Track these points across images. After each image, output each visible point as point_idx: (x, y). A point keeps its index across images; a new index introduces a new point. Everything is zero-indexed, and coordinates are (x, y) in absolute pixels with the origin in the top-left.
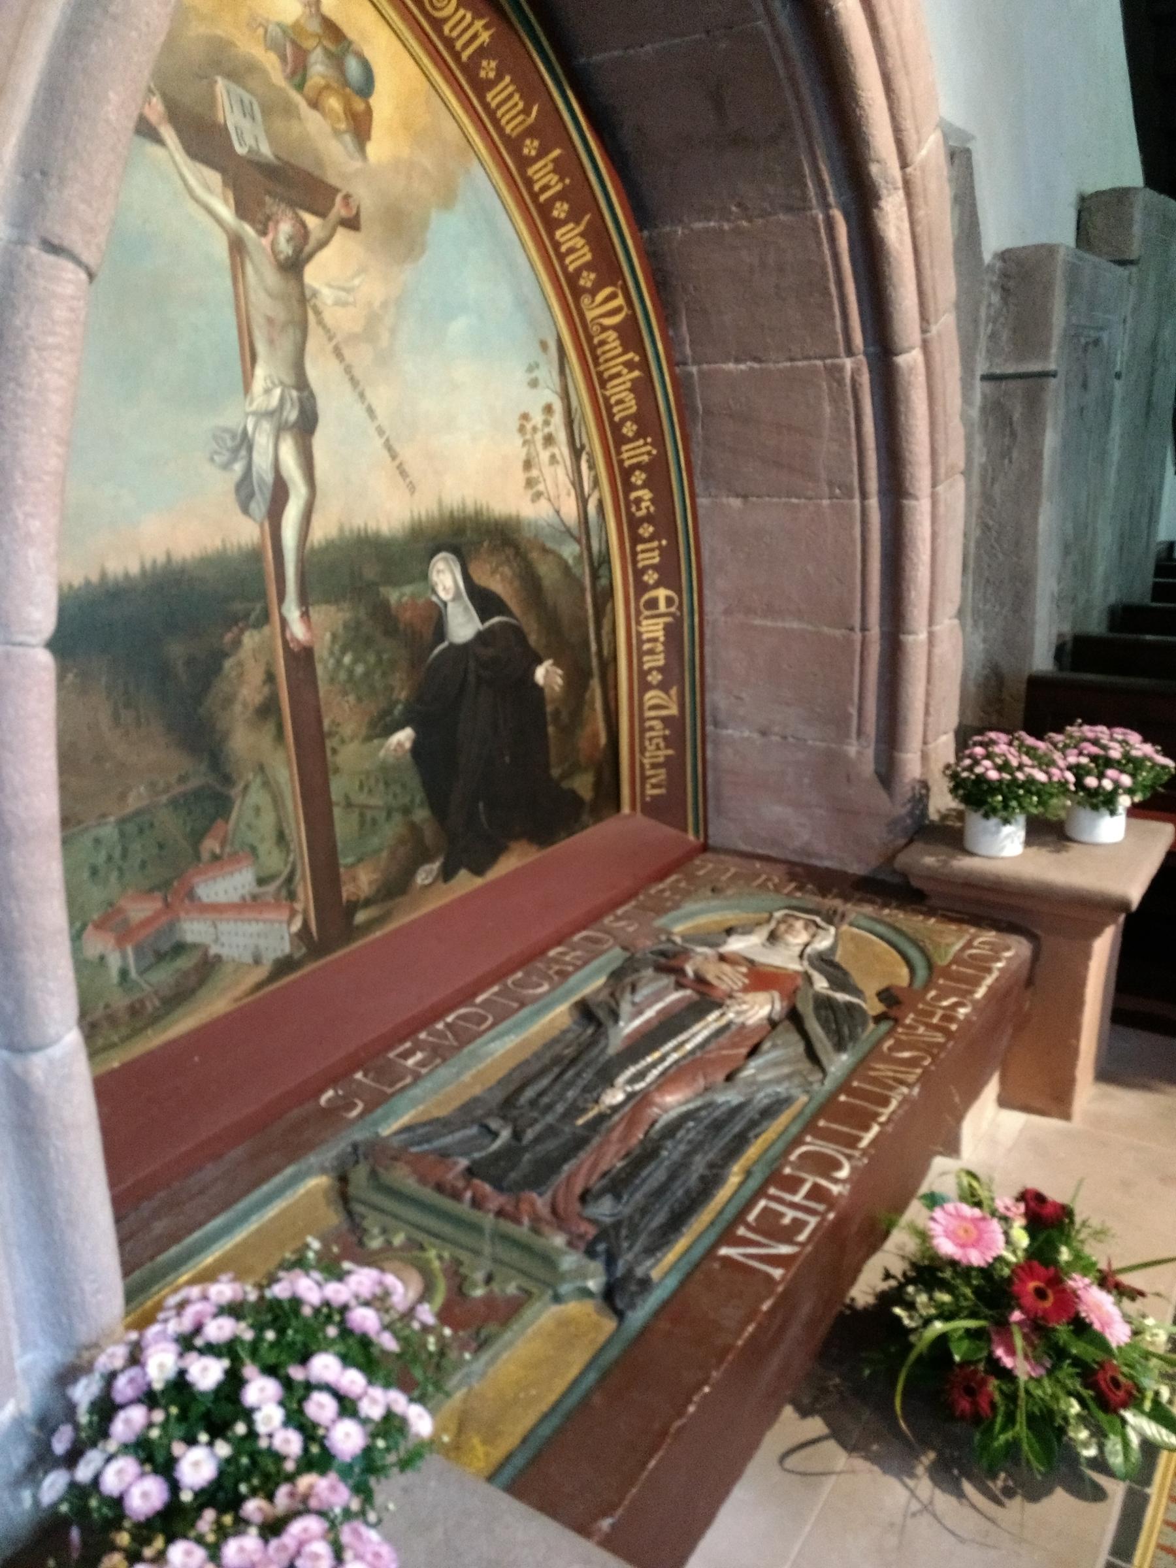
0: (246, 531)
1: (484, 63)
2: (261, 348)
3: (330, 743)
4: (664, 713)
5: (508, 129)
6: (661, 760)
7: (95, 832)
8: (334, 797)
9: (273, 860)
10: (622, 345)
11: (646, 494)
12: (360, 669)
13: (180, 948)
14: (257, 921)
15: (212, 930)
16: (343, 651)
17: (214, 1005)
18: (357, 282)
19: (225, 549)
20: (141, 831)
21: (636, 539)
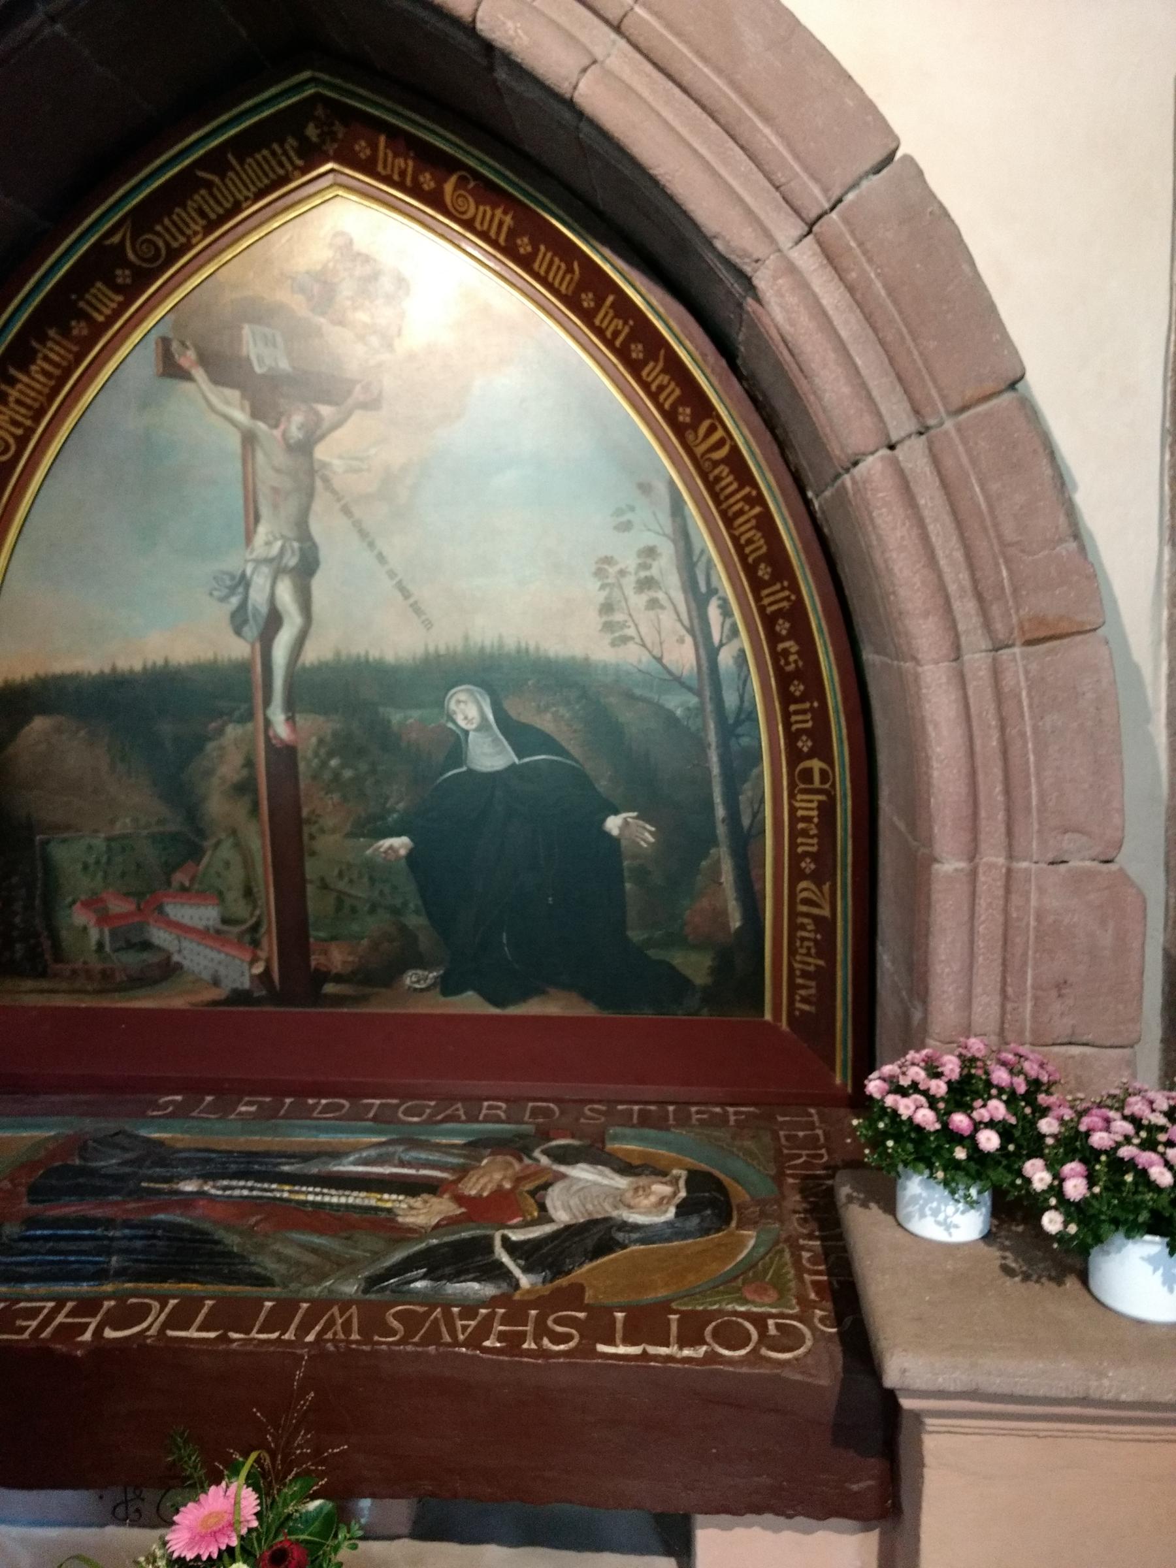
0: (238, 649)
1: (519, 242)
2: (265, 510)
3: (306, 830)
4: (815, 911)
5: (563, 289)
6: (812, 968)
8: (308, 877)
9: (240, 909)
10: (736, 479)
12: (348, 774)
13: (147, 946)
15: (176, 942)
16: (331, 754)
20: (124, 849)
21: (787, 698)
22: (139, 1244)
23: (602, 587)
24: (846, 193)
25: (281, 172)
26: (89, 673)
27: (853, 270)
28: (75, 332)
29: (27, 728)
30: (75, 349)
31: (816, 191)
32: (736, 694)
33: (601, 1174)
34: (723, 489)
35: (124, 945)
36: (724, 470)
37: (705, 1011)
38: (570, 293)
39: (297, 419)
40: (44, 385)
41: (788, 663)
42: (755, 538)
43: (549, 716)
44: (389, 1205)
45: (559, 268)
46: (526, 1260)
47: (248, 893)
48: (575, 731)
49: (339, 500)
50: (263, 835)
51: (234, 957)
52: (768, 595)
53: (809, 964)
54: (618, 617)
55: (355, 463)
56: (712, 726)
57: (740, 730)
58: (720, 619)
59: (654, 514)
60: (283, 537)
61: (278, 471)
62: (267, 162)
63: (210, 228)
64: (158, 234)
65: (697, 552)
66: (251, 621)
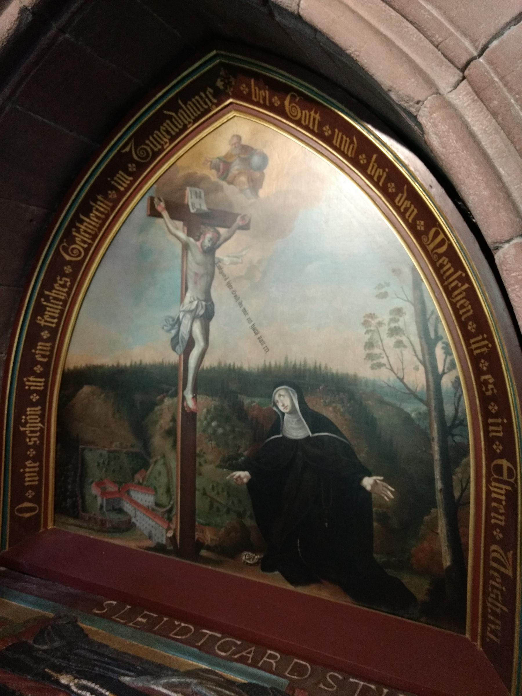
0: (173, 357)
1: (324, 129)
2: (190, 285)
3: (198, 460)
4: (503, 570)
6: (498, 611)
8: (197, 486)
9: (164, 499)
10: (452, 266)
12: (220, 431)
13: (121, 511)
15: (134, 511)
16: (213, 419)
18: (244, 253)
20: (115, 459)
21: (487, 414)
23: (367, 332)
24: (490, 41)
25: (206, 107)
26: (108, 366)
27: (494, 99)
28: (110, 196)
30: (111, 204)
31: (467, 44)
34: (445, 272)
35: (111, 509)
36: (445, 260)
38: (353, 156)
39: (209, 236)
40: (97, 223)
41: (487, 390)
42: (466, 305)
43: (331, 409)
45: (346, 141)
47: (168, 491)
48: (346, 420)
49: (226, 279)
52: (474, 343)
54: (376, 351)
55: (235, 259)
56: (435, 426)
57: (455, 431)
58: (444, 356)
59: (402, 288)
60: (198, 299)
61: (197, 264)
62: (198, 102)
63: (173, 139)
64: (148, 145)
65: (429, 312)
66: (180, 344)
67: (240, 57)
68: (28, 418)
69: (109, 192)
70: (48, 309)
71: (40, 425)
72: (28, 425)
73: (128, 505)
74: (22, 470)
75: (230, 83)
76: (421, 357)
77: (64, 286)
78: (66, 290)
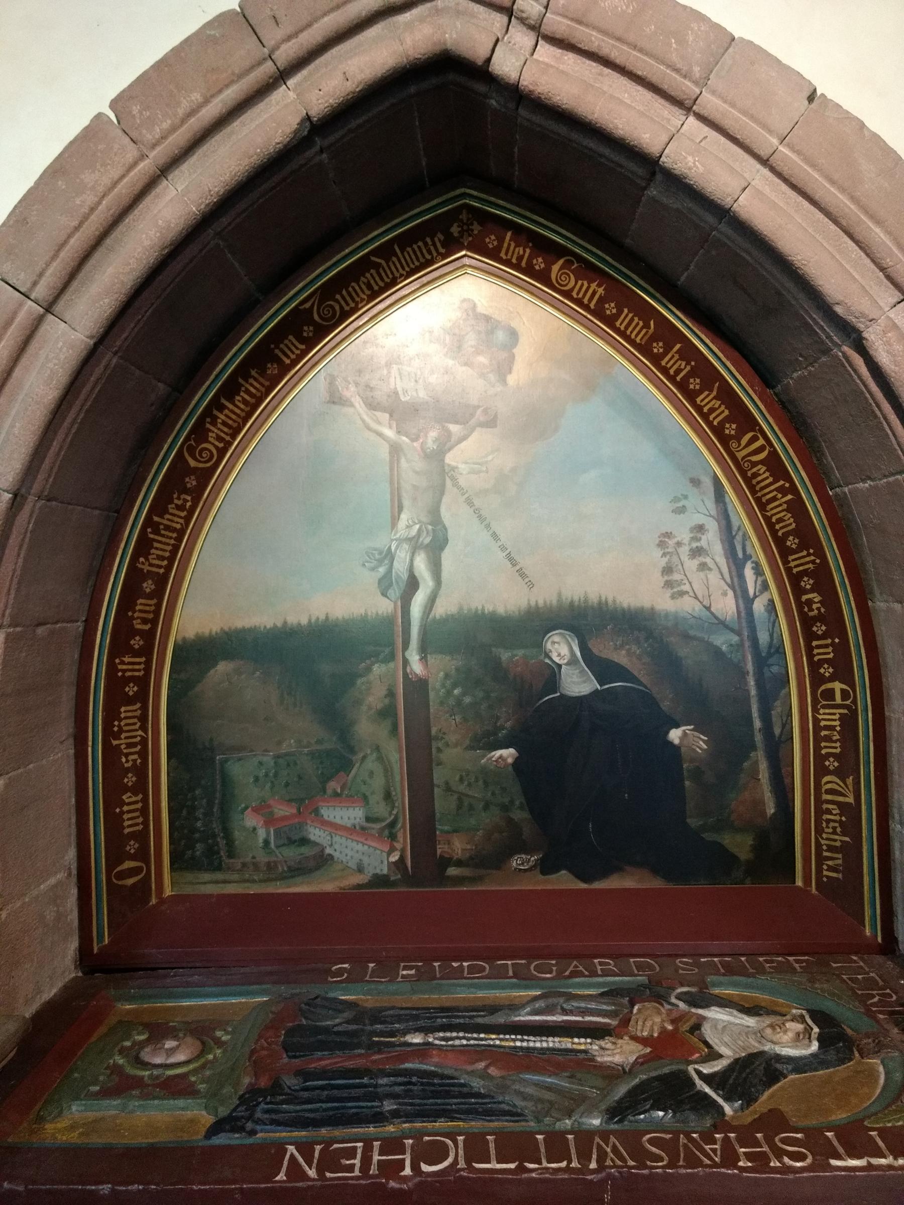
0: (384, 606)
1: (607, 306)
2: (406, 503)
3: (434, 745)
4: (841, 799)
6: (838, 844)
7: (260, 758)
8: (436, 782)
9: (381, 809)
11: (815, 597)
12: (467, 700)
13: (304, 841)
14: (364, 844)
15: (329, 838)
16: (455, 686)
17: (328, 886)
18: (490, 458)
19: (366, 614)
20: (288, 765)
21: (810, 636)
22: (398, 1089)
23: (664, 555)
25: (429, 257)
28: (269, 372)
29: (212, 672)
30: (267, 383)
32: (768, 633)
33: (731, 1014)
34: (758, 483)
37: (748, 880)
41: (811, 610)
43: (624, 652)
44: (583, 1047)
46: (723, 1090)
48: (644, 664)
49: (463, 494)
50: (400, 752)
51: (376, 849)
52: (793, 560)
53: (835, 840)
54: (676, 577)
57: (771, 661)
58: (754, 577)
60: (420, 522)
61: (417, 473)
64: (337, 301)
65: (735, 528)
67: (501, 202)
68: (122, 723)
69: (269, 365)
70: (156, 545)
71: (140, 733)
72: (123, 736)
73: (317, 832)
74: (118, 810)
75: (470, 232)
76: (729, 580)
77: (180, 508)
78: (183, 514)
